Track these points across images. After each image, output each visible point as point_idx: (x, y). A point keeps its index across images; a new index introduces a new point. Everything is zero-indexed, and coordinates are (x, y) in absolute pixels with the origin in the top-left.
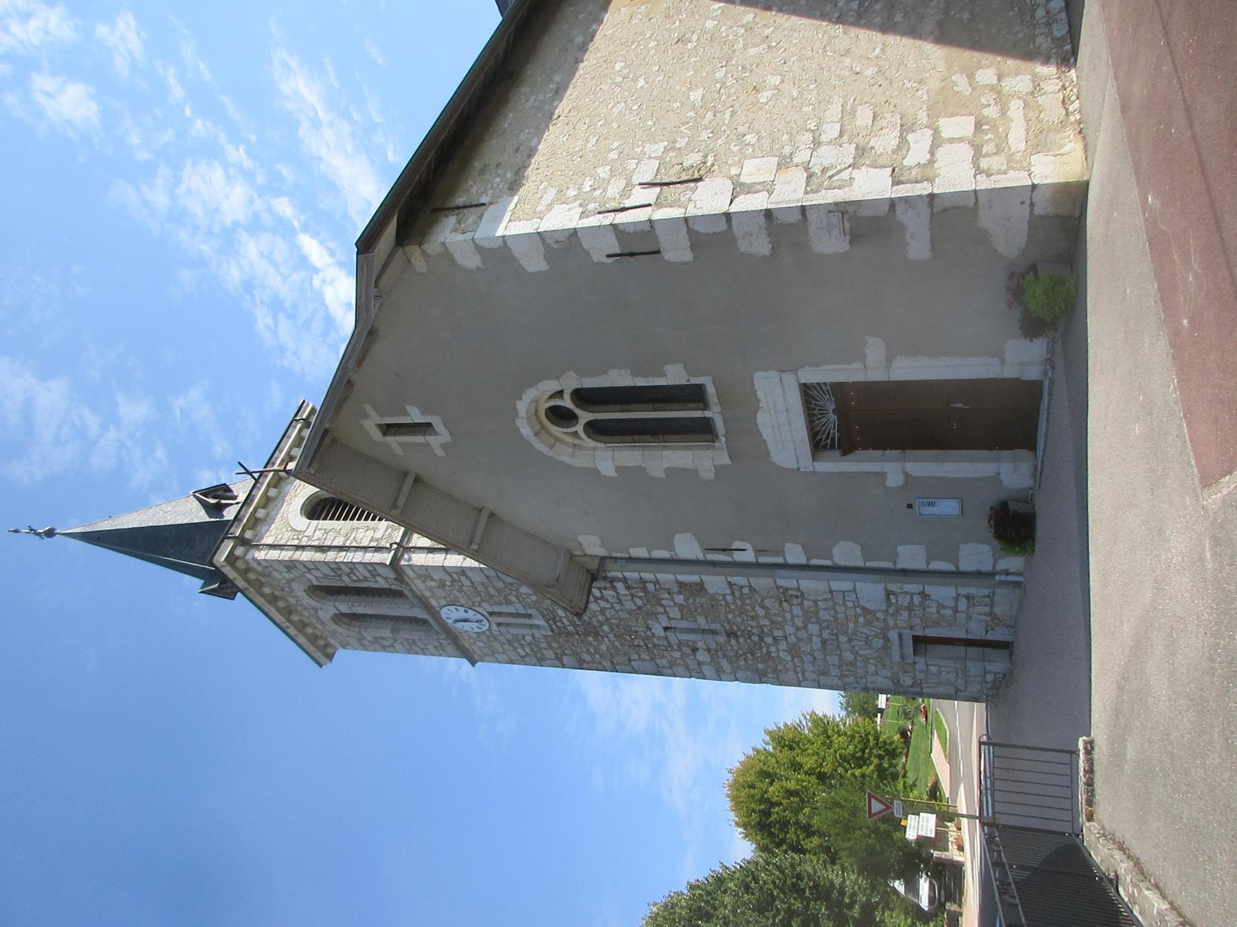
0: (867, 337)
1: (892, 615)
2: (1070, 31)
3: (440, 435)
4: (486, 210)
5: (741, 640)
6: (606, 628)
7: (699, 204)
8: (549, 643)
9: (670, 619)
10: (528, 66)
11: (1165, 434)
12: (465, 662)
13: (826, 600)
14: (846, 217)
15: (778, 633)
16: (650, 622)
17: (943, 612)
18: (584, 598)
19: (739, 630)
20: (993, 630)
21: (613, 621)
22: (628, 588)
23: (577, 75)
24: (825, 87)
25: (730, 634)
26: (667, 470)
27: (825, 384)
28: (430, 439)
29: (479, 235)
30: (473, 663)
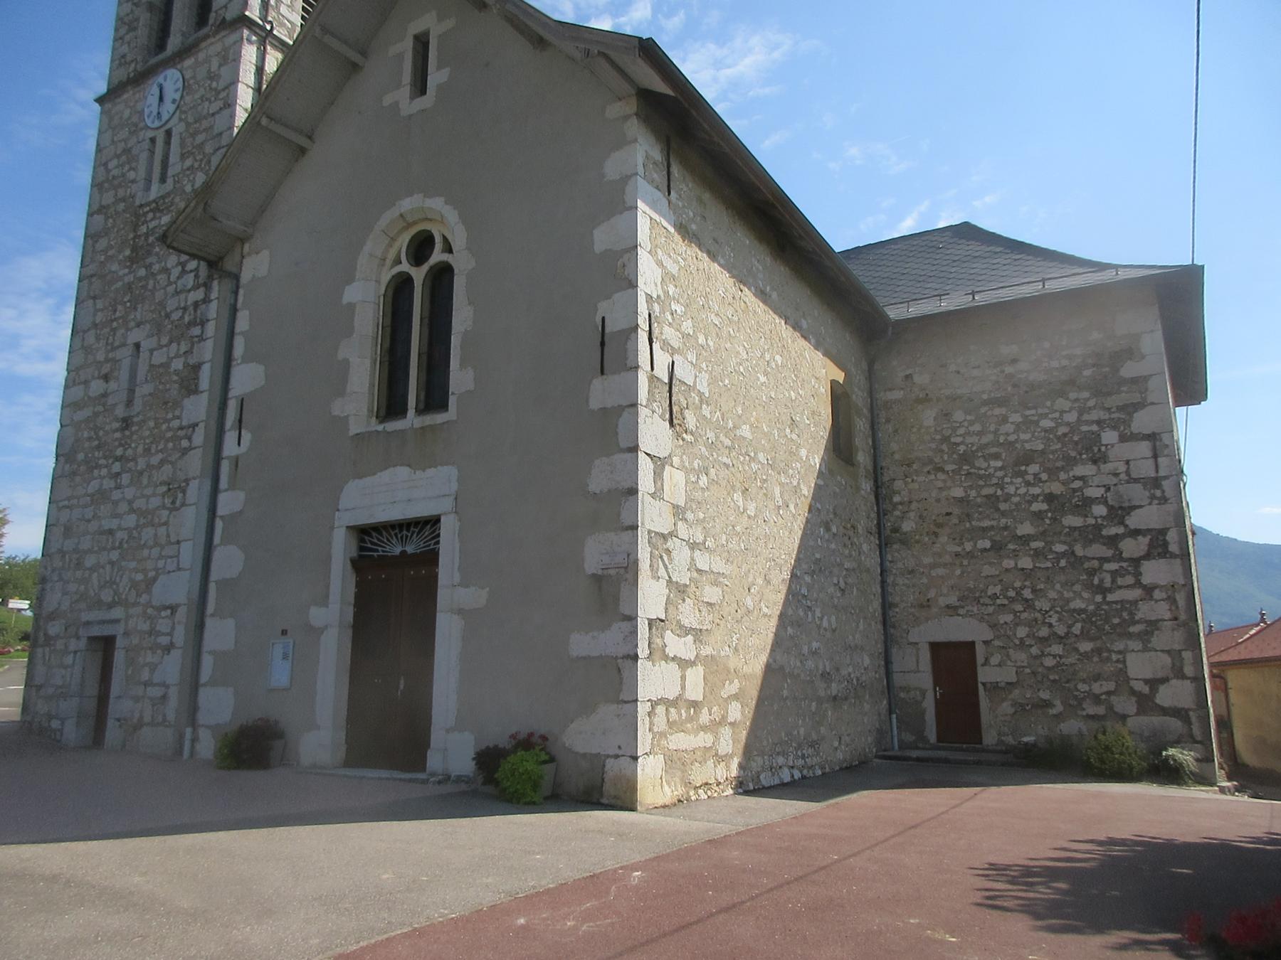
0: (488, 589)
1: (145, 612)
2: (764, 788)
3: (410, 103)
4: (664, 195)
5: (118, 435)
6: (142, 272)
7: (649, 420)
8: (123, 200)
9: (151, 351)
10: (787, 269)
11: (389, 909)
12: (102, 88)
13: (168, 536)
14: (622, 571)
15: (125, 479)
16: (148, 326)
17: (147, 669)
18: (186, 248)
19: (132, 434)
20: (120, 726)
21: (151, 282)
22: (196, 305)
23: (775, 316)
24: (740, 558)
25: (126, 423)
26: (346, 362)
27: (438, 543)
28: (406, 91)
29: (641, 182)
30: (100, 100)
